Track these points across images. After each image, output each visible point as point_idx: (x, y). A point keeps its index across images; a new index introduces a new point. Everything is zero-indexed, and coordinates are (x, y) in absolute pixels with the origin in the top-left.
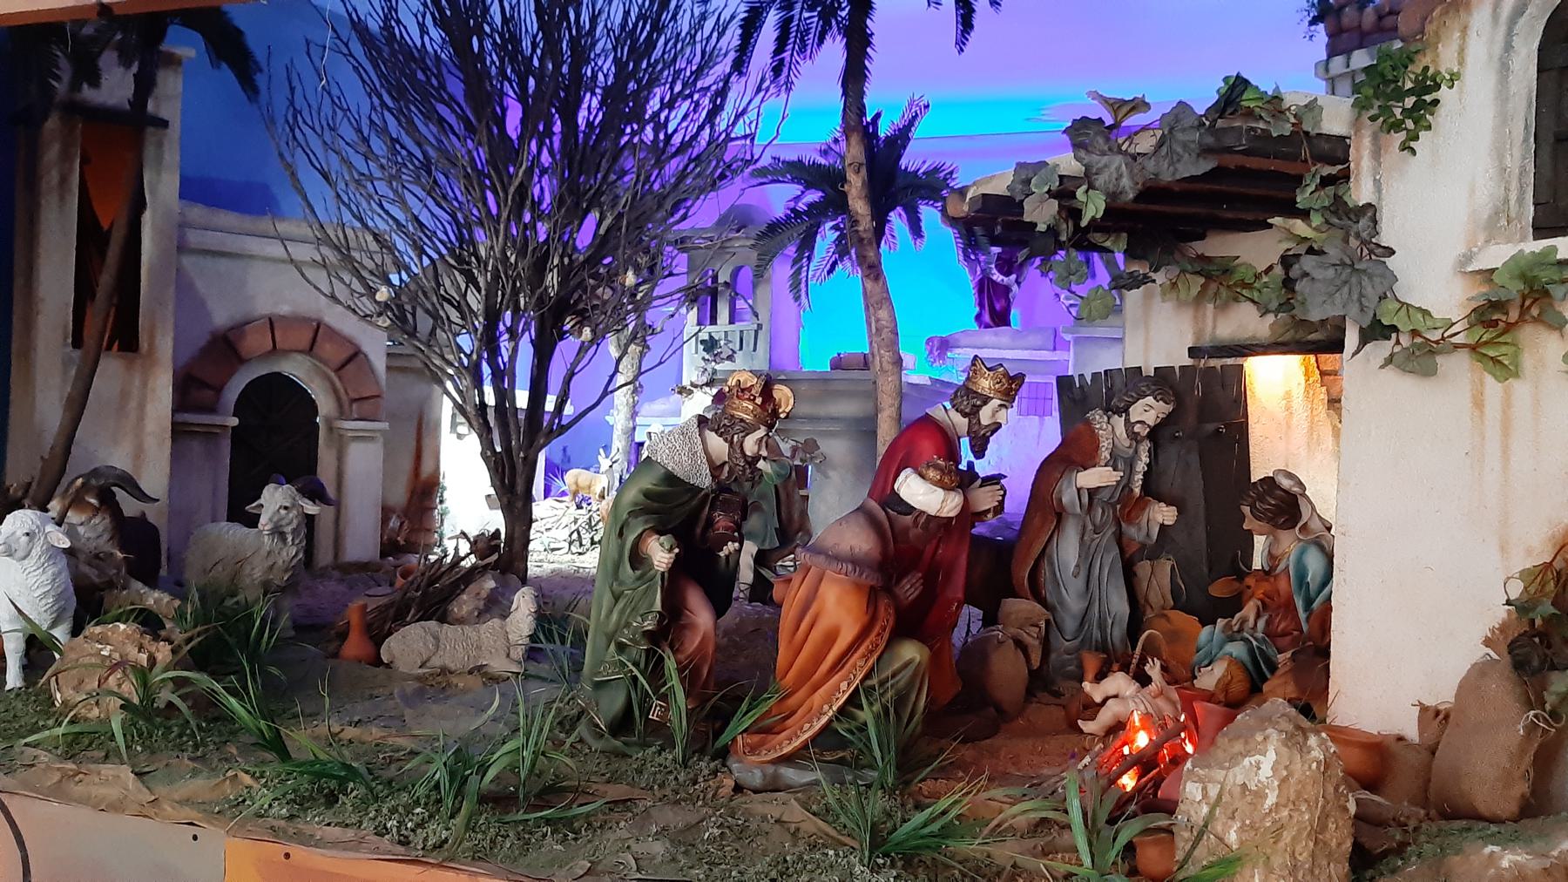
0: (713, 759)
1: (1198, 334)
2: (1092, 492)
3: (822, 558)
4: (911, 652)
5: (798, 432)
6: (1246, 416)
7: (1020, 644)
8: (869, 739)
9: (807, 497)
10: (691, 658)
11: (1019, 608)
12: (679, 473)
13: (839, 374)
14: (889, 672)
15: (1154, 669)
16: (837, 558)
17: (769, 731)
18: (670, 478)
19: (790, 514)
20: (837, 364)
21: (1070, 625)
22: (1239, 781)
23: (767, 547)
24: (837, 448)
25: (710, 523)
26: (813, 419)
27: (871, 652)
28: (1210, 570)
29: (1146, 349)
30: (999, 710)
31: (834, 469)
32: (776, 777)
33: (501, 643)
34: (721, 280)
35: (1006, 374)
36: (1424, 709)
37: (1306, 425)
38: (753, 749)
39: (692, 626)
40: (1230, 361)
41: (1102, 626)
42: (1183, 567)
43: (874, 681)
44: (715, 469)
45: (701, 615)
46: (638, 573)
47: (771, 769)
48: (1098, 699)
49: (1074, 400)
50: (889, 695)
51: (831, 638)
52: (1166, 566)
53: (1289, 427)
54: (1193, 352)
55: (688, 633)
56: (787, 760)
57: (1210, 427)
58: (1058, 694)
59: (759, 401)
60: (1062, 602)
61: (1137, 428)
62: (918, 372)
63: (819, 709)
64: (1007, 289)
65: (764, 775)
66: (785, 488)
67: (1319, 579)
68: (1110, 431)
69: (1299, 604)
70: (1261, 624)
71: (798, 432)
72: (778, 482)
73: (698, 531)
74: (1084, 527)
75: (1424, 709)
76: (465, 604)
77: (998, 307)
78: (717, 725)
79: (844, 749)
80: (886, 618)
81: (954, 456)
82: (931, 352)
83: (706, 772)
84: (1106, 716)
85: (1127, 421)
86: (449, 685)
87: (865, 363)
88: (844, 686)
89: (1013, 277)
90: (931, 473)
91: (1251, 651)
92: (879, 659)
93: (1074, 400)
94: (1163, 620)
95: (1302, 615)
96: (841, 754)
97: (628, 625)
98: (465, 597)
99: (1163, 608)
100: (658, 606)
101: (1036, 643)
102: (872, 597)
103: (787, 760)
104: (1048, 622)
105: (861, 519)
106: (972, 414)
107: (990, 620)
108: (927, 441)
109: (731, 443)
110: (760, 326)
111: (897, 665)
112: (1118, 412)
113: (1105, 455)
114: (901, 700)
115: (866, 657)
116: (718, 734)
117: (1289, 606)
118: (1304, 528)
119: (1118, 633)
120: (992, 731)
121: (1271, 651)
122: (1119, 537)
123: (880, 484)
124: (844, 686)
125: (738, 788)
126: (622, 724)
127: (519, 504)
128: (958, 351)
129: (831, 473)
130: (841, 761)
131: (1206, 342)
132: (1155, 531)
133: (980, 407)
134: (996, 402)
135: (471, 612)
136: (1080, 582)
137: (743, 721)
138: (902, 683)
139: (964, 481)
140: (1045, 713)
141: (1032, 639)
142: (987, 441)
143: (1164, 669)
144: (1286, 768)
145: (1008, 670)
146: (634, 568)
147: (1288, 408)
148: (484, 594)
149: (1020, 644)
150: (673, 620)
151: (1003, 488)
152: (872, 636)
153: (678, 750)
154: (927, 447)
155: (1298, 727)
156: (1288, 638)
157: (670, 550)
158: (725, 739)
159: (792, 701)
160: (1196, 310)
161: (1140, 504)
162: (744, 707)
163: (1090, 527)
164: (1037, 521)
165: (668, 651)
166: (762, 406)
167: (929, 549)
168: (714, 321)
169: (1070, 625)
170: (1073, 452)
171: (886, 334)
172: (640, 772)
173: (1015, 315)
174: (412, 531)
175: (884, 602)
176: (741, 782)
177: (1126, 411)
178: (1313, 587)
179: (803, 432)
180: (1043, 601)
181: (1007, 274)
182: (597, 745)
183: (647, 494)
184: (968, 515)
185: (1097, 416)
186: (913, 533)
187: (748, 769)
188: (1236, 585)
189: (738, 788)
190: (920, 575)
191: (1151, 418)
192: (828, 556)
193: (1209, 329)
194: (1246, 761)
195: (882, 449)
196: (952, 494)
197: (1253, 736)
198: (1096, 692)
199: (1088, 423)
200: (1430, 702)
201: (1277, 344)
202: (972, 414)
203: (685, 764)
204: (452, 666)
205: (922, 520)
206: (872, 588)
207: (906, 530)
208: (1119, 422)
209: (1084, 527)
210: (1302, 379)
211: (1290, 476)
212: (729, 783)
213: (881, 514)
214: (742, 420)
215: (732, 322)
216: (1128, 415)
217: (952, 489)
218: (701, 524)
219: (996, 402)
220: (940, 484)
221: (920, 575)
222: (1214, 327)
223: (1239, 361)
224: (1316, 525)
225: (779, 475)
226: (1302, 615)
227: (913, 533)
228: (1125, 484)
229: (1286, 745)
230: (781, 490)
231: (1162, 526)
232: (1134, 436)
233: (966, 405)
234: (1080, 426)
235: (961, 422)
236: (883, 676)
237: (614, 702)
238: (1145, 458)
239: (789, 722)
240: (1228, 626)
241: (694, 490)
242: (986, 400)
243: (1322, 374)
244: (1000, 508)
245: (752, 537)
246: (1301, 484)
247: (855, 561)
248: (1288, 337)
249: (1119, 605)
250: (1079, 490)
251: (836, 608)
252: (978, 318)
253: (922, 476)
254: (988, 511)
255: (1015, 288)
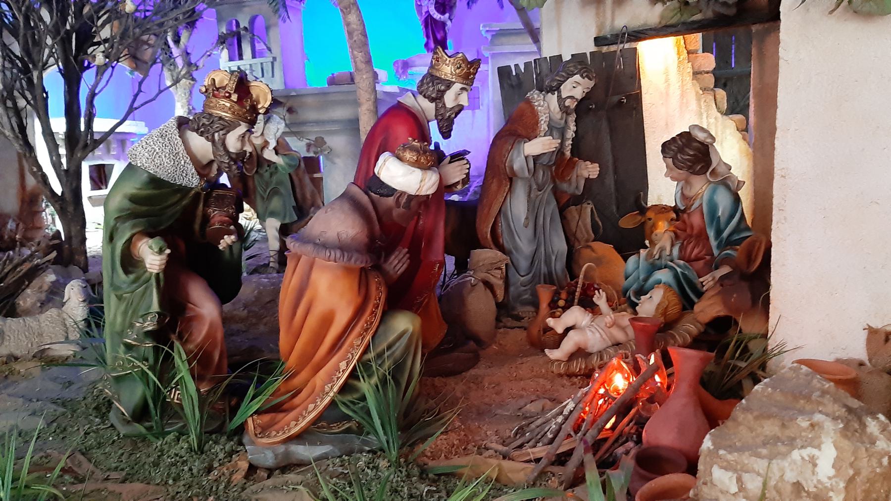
0: (230, 439)
1: (600, 27)
2: (536, 158)
3: (309, 248)
4: (404, 323)
5: (308, 132)
6: (640, 87)
7: (488, 285)
8: (368, 413)
9: (321, 179)
10: (200, 347)
11: (484, 256)
12: (162, 174)
13: (334, 88)
14: (384, 345)
15: (600, 299)
16: (325, 246)
17: (278, 409)
18: (155, 182)
19: (304, 196)
20: (332, 81)
21: (523, 264)
22: (791, 476)
23: (287, 221)
24: (338, 142)
25: (206, 219)
26: (317, 123)
27: (366, 330)
28: (618, 208)
29: (560, 43)
30: (478, 341)
31: (338, 156)
32: (287, 454)
33: (59, 330)
34: (242, 26)
35: (465, 60)
36: (872, 332)
37: (678, 92)
38: (264, 430)
39: (198, 318)
40: (627, 46)
41: (548, 262)
42: (599, 209)
43: (371, 355)
44: (203, 168)
45: (205, 306)
46: (132, 277)
47: (281, 449)
48: (560, 330)
49: (512, 86)
50: (387, 364)
51: (327, 321)
52: (588, 208)
53: (667, 94)
54: (598, 41)
55: (194, 324)
56: (299, 438)
57: (615, 99)
58: (519, 318)
59: (234, 97)
60: (517, 248)
61: (568, 103)
62: (389, 85)
63: (324, 387)
64: (444, 24)
65: (276, 456)
66: (297, 175)
67: (727, 214)
68: (547, 106)
69: (711, 234)
70: (676, 251)
71: (308, 132)
72: (291, 171)
73: (197, 227)
74: (530, 187)
75: (872, 332)
76: (28, 298)
77: (439, 36)
78: (233, 403)
79: (349, 422)
80: (378, 295)
81: (424, 137)
82: (397, 71)
83: (221, 456)
84: (568, 345)
85: (559, 97)
86: (12, 372)
87: (351, 79)
88: (343, 365)
89: (447, 15)
90: (408, 155)
91: (676, 276)
92: (373, 337)
93: (512, 86)
94: (588, 251)
95: (713, 243)
96: (347, 426)
97: (132, 326)
98: (28, 291)
99: (587, 241)
100: (155, 307)
101: (501, 282)
102: (363, 277)
103: (299, 438)
104: (507, 265)
105: (346, 206)
106: (438, 99)
107: (462, 266)
108: (398, 126)
109: (213, 141)
110: (275, 59)
111: (392, 338)
112: (551, 90)
113: (544, 126)
114: (398, 368)
115: (361, 336)
116: (234, 411)
117: (702, 236)
118: (713, 173)
119: (559, 266)
120: (475, 361)
121: (692, 275)
122: (556, 192)
123: (364, 167)
124: (343, 365)
125: (253, 468)
126: (141, 414)
127: (71, 209)
128: (414, 69)
129: (337, 161)
130: (348, 431)
131: (607, 32)
132: (582, 183)
133: (444, 92)
134: (457, 87)
135: (34, 304)
136: (530, 231)
137: (249, 408)
138: (398, 353)
139: (436, 159)
140: (514, 337)
141: (498, 282)
142: (453, 123)
143: (609, 300)
144: (851, 465)
145: (480, 307)
146: (127, 272)
147: (667, 81)
148: (46, 287)
149: (488, 285)
150: (174, 315)
151: (468, 162)
152: (366, 316)
153: (193, 437)
154: (401, 131)
155: (850, 410)
156: (701, 262)
157: (161, 251)
158: (237, 421)
159: (297, 381)
160: (598, 8)
161: (570, 165)
162: (251, 391)
163: (534, 187)
164: (494, 186)
165: (177, 344)
166: (240, 101)
167: (412, 224)
168: (241, 57)
169: (523, 264)
170: (516, 126)
171: (357, 37)
172: (156, 464)
173: (449, 42)
174: (26, 229)
175: (375, 282)
176: (254, 463)
177: (558, 88)
178: (723, 220)
179: (314, 132)
180: (501, 248)
181: (443, 13)
182: (123, 430)
183: (133, 199)
184: (444, 188)
185: (535, 96)
186: (396, 212)
187: (262, 449)
188: (639, 218)
189: (253, 468)
190: (403, 253)
191: (579, 93)
192: (315, 244)
193: (608, 23)
194: (796, 454)
195: (363, 138)
196: (429, 173)
197: (793, 419)
198: (558, 325)
199: (529, 102)
200: (877, 324)
201: (666, 26)
202: (438, 99)
203: (201, 450)
204: (18, 353)
205: (403, 200)
206: (362, 269)
207: (389, 210)
208: (553, 99)
209: (530, 187)
210: (676, 57)
211: (702, 129)
212: (244, 465)
213: (364, 199)
214: (221, 118)
215: (254, 57)
216: (559, 92)
217: (429, 168)
218: (198, 221)
219: (457, 87)
220: (417, 164)
221: (403, 253)
222: (613, 20)
223: (633, 45)
224: (721, 169)
225: (290, 166)
226: (713, 243)
227: (396, 212)
228: (560, 151)
229: (845, 436)
230: (294, 177)
231: (588, 180)
232: (565, 110)
233: (432, 91)
234: (522, 105)
235: (428, 107)
236: (379, 349)
237: (135, 393)
238: (572, 127)
239: (297, 400)
240: (650, 255)
241: (183, 190)
242: (449, 85)
243: (688, 53)
244: (466, 180)
245: (273, 214)
246: (714, 139)
247: (343, 247)
248: (673, 21)
249: (560, 245)
250: (526, 158)
251: (325, 292)
252: (427, 45)
253: (400, 159)
254: (458, 183)
255: (449, 23)
